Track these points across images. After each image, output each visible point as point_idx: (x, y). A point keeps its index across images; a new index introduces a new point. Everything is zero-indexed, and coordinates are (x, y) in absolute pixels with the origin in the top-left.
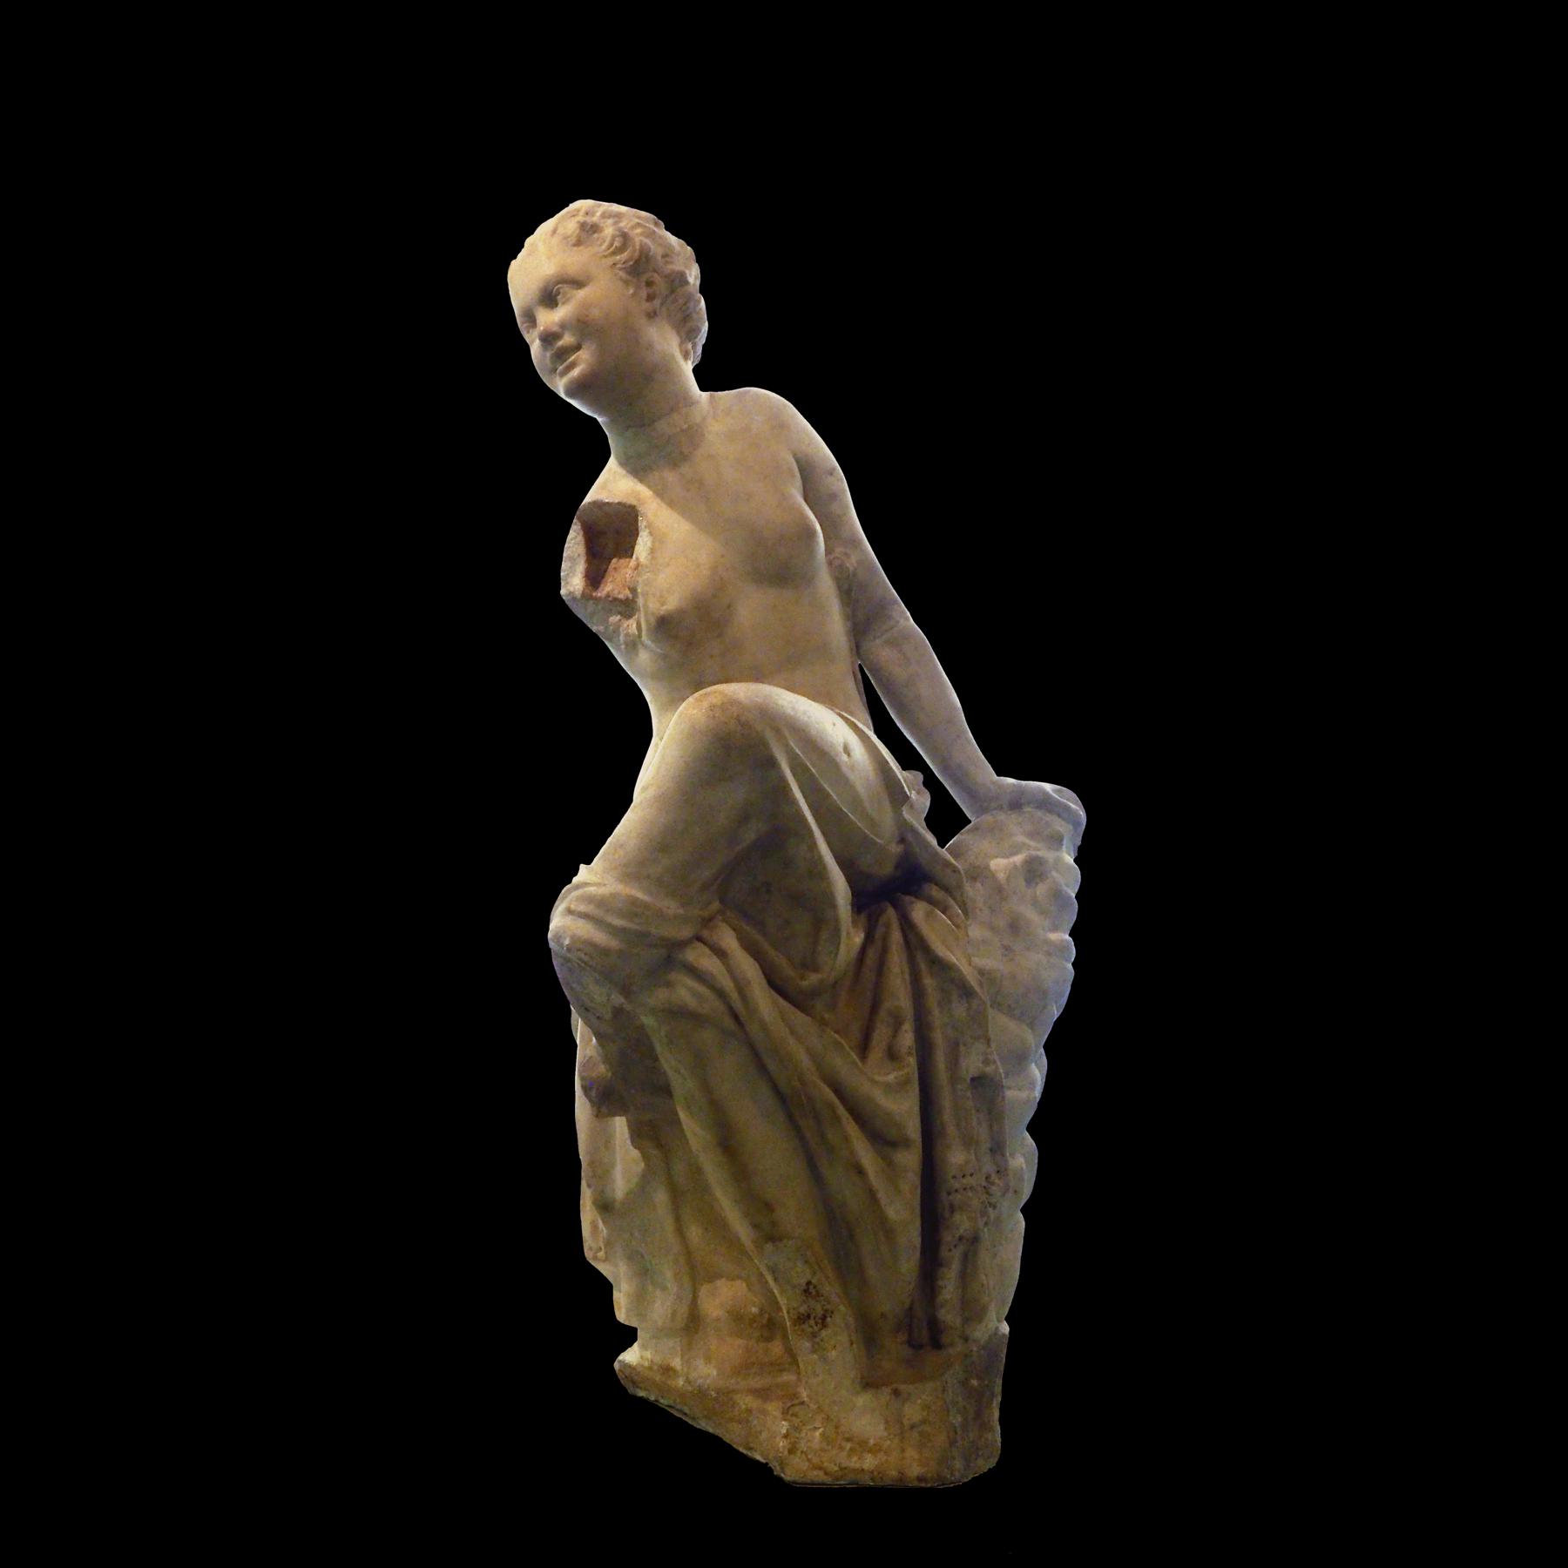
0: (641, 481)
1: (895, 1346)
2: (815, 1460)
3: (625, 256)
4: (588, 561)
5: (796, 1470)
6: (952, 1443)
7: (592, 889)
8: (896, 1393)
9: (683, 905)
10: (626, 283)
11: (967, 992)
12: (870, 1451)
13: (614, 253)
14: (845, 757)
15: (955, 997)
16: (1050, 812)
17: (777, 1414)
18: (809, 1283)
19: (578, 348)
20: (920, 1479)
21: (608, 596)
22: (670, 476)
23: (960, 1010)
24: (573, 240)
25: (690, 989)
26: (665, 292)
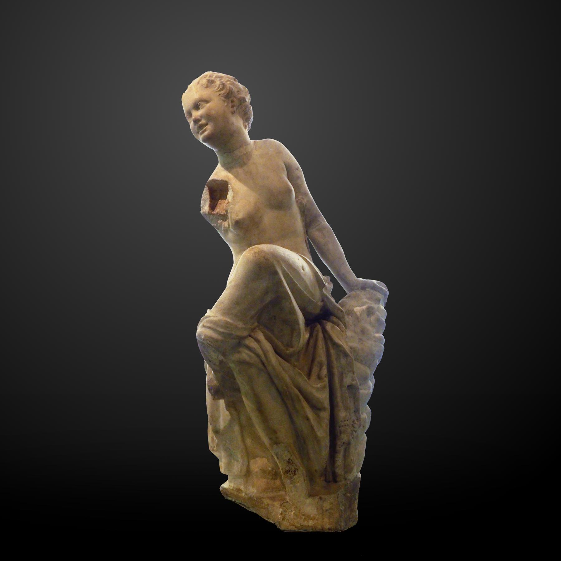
0: (229, 172)
1: (320, 482)
2: (292, 522)
3: (224, 91)
4: (211, 201)
5: (285, 526)
6: (341, 516)
7: (212, 318)
8: (321, 498)
9: (244, 324)
10: (224, 101)
11: (346, 355)
12: (311, 519)
13: (220, 91)
14: (302, 271)
15: (342, 357)
16: (376, 290)
17: (278, 506)
18: (289, 459)
19: (207, 124)
20: (329, 529)
21: (217, 213)
22: (240, 170)
23: (343, 361)
24: (205, 86)
25: (247, 354)
26: (238, 104)
